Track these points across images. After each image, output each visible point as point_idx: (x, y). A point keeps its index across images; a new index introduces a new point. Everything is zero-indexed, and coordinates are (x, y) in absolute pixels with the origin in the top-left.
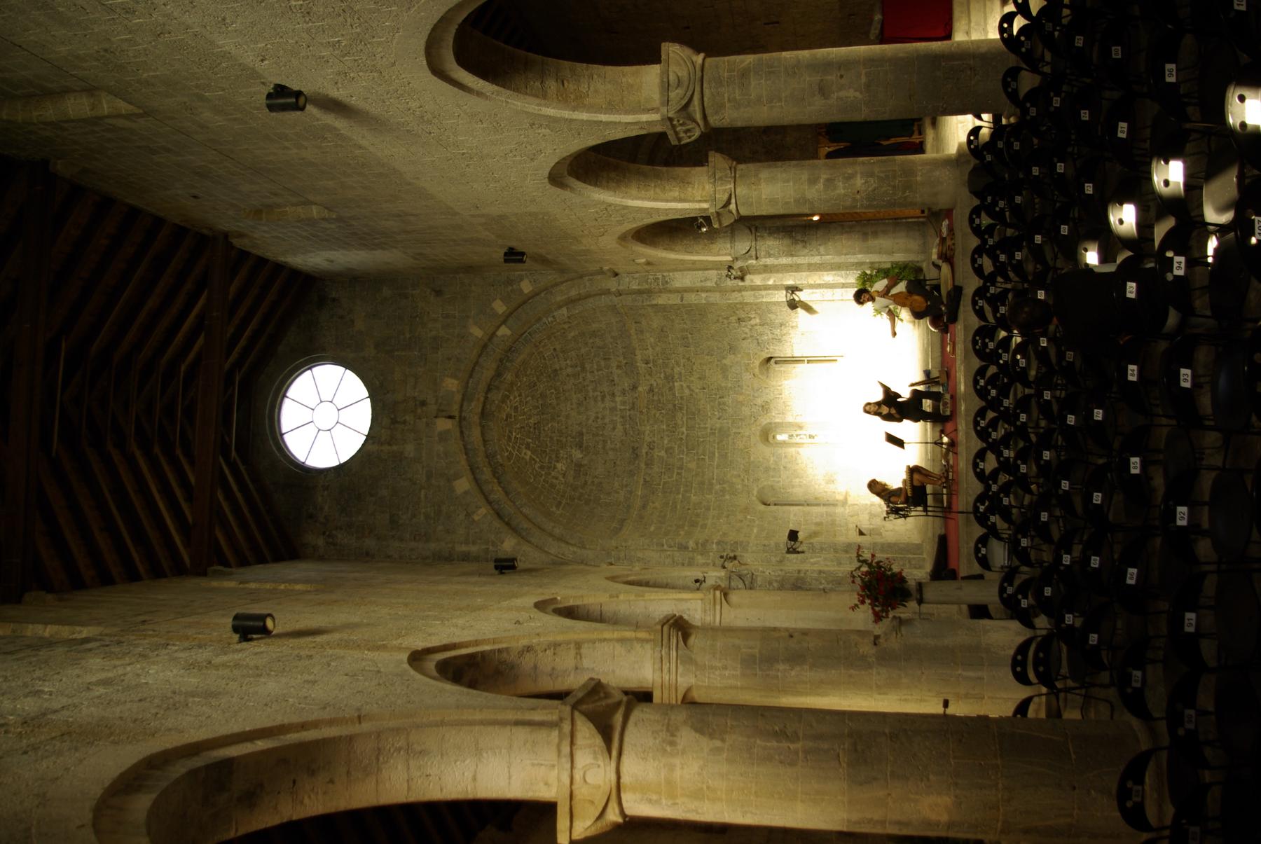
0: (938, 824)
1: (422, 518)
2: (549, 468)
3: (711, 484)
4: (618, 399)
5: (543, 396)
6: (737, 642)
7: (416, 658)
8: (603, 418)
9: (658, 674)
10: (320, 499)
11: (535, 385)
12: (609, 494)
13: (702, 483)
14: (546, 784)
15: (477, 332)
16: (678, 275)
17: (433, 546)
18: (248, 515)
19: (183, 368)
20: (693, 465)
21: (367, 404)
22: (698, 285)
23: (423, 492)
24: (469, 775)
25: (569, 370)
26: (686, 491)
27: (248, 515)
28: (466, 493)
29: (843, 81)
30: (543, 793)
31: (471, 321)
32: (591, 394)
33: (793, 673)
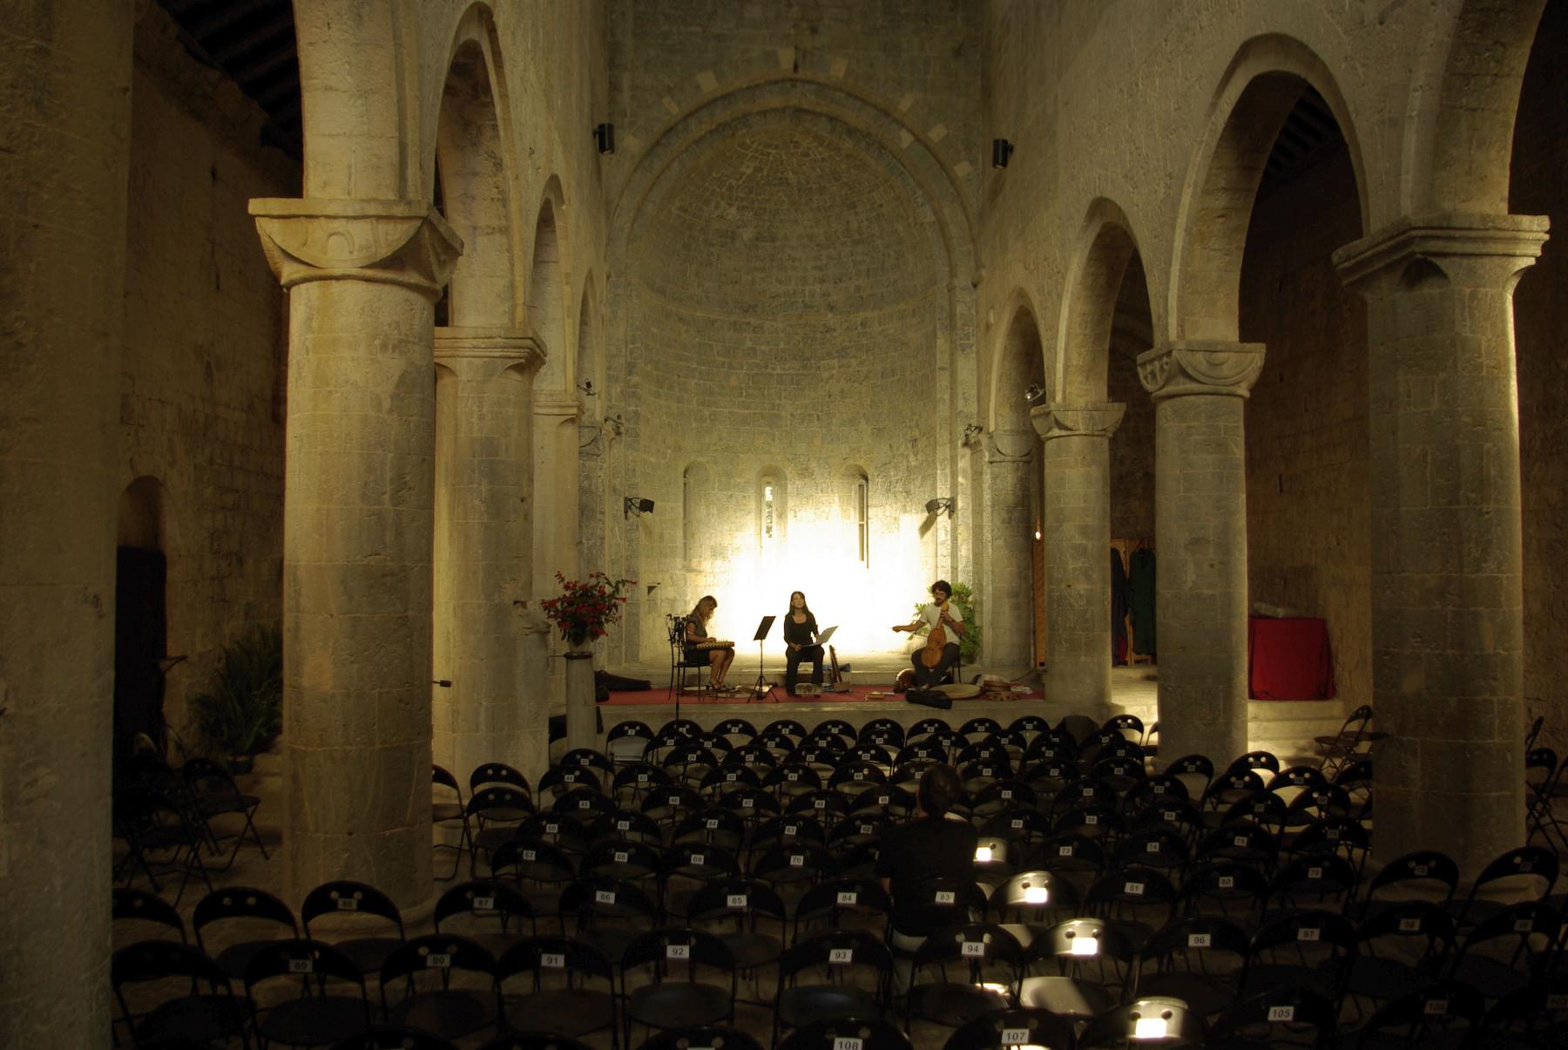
4: (817, 287)
14: (325, 184)
16: (973, 363)
20: (734, 382)
23: (699, 29)
25: (854, 225)
28: (698, 87)
33: (477, 502)
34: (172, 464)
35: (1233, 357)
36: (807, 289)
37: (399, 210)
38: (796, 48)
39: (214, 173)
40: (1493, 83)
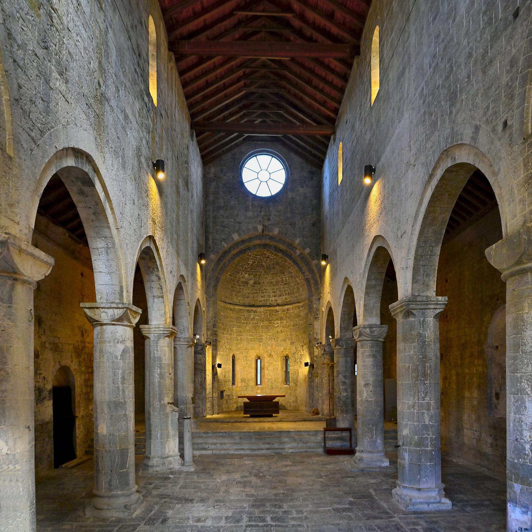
0: (97, 430)
4: (273, 298)
5: (274, 268)
6: (167, 355)
7: (151, 238)
9: (154, 326)
10: (229, 175)
12: (236, 295)
13: (241, 332)
14: (101, 298)
15: (297, 241)
17: (211, 224)
18: (221, 143)
19: (281, 112)
20: (248, 328)
21: (269, 195)
22: (315, 331)
24: (101, 270)
25: (284, 279)
27: (221, 143)
28: (233, 238)
29: (369, 392)
31: (302, 239)
32: (275, 287)
34: (72, 361)
35: (378, 329)
37: (120, 306)
39: (82, 274)
40: (430, 257)
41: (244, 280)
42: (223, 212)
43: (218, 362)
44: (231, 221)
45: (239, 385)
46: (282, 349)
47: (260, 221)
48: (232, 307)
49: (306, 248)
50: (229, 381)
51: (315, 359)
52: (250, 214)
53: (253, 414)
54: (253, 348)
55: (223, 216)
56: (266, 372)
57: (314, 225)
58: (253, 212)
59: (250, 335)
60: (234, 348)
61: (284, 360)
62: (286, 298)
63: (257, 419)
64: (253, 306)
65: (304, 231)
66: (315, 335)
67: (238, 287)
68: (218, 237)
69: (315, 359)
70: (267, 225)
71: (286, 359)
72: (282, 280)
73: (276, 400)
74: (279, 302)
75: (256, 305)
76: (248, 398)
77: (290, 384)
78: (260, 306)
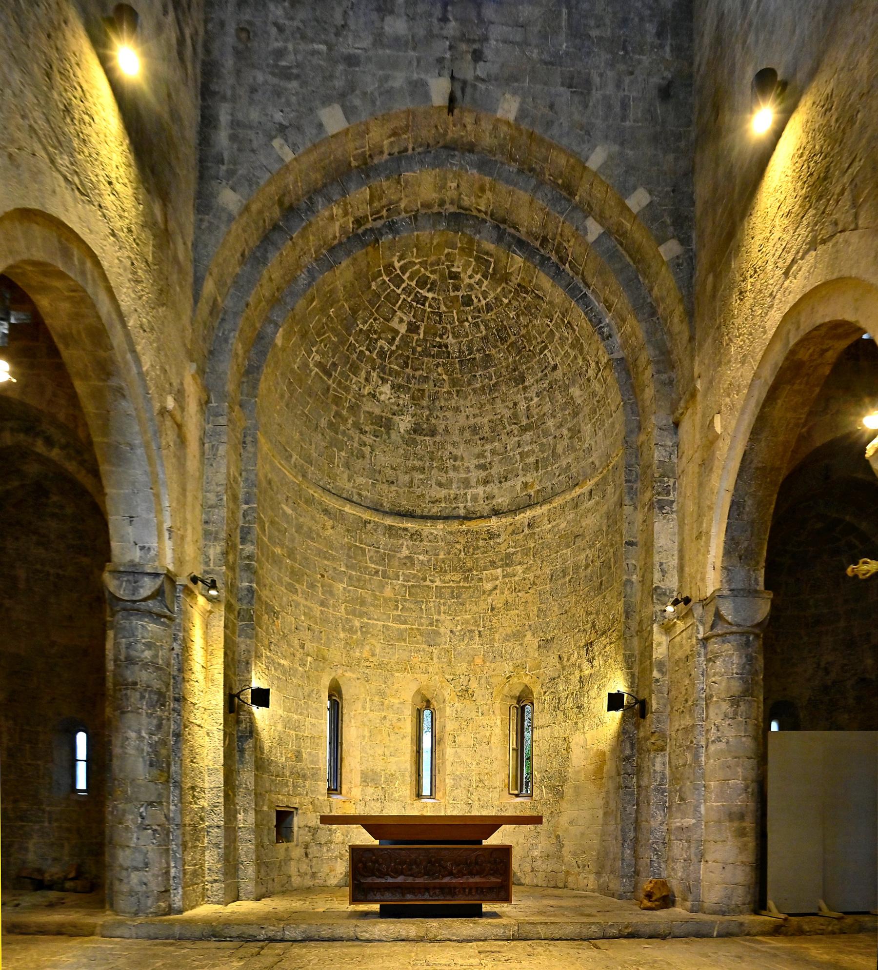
1: (279, 45)
2: (383, 369)
3: (361, 615)
4: (480, 490)
8: (455, 469)
11: (503, 340)
12: (347, 466)
15: (596, 159)
16: (673, 526)
17: (229, 63)
20: (388, 592)
22: (656, 558)
23: (323, 47)
25: (522, 406)
26: (350, 578)
28: (320, 126)
30: (507, 843)
31: (616, 148)
32: (488, 447)
36: (470, 492)
38: (453, 78)
41: (377, 411)
42: (280, 12)
43: (258, 681)
44: (314, 53)
45: (357, 793)
46: (508, 667)
47: (440, 60)
48: (333, 503)
49: (635, 188)
50: (315, 775)
51: (656, 674)
52: (397, 26)
53: (394, 901)
54: (407, 667)
55: (281, 29)
56: (449, 752)
57: (665, 93)
58: (411, 18)
59: (398, 619)
60: (335, 654)
61: (514, 712)
62: (525, 485)
63: (410, 927)
64: (410, 515)
65: (624, 118)
66: (657, 576)
67: (356, 436)
68: (254, 115)
69: (656, 674)
70: (469, 76)
71: (522, 704)
72: (515, 415)
73: (494, 840)
74: (502, 500)
75: (419, 512)
76: (373, 825)
77: (536, 792)
78: (434, 518)
